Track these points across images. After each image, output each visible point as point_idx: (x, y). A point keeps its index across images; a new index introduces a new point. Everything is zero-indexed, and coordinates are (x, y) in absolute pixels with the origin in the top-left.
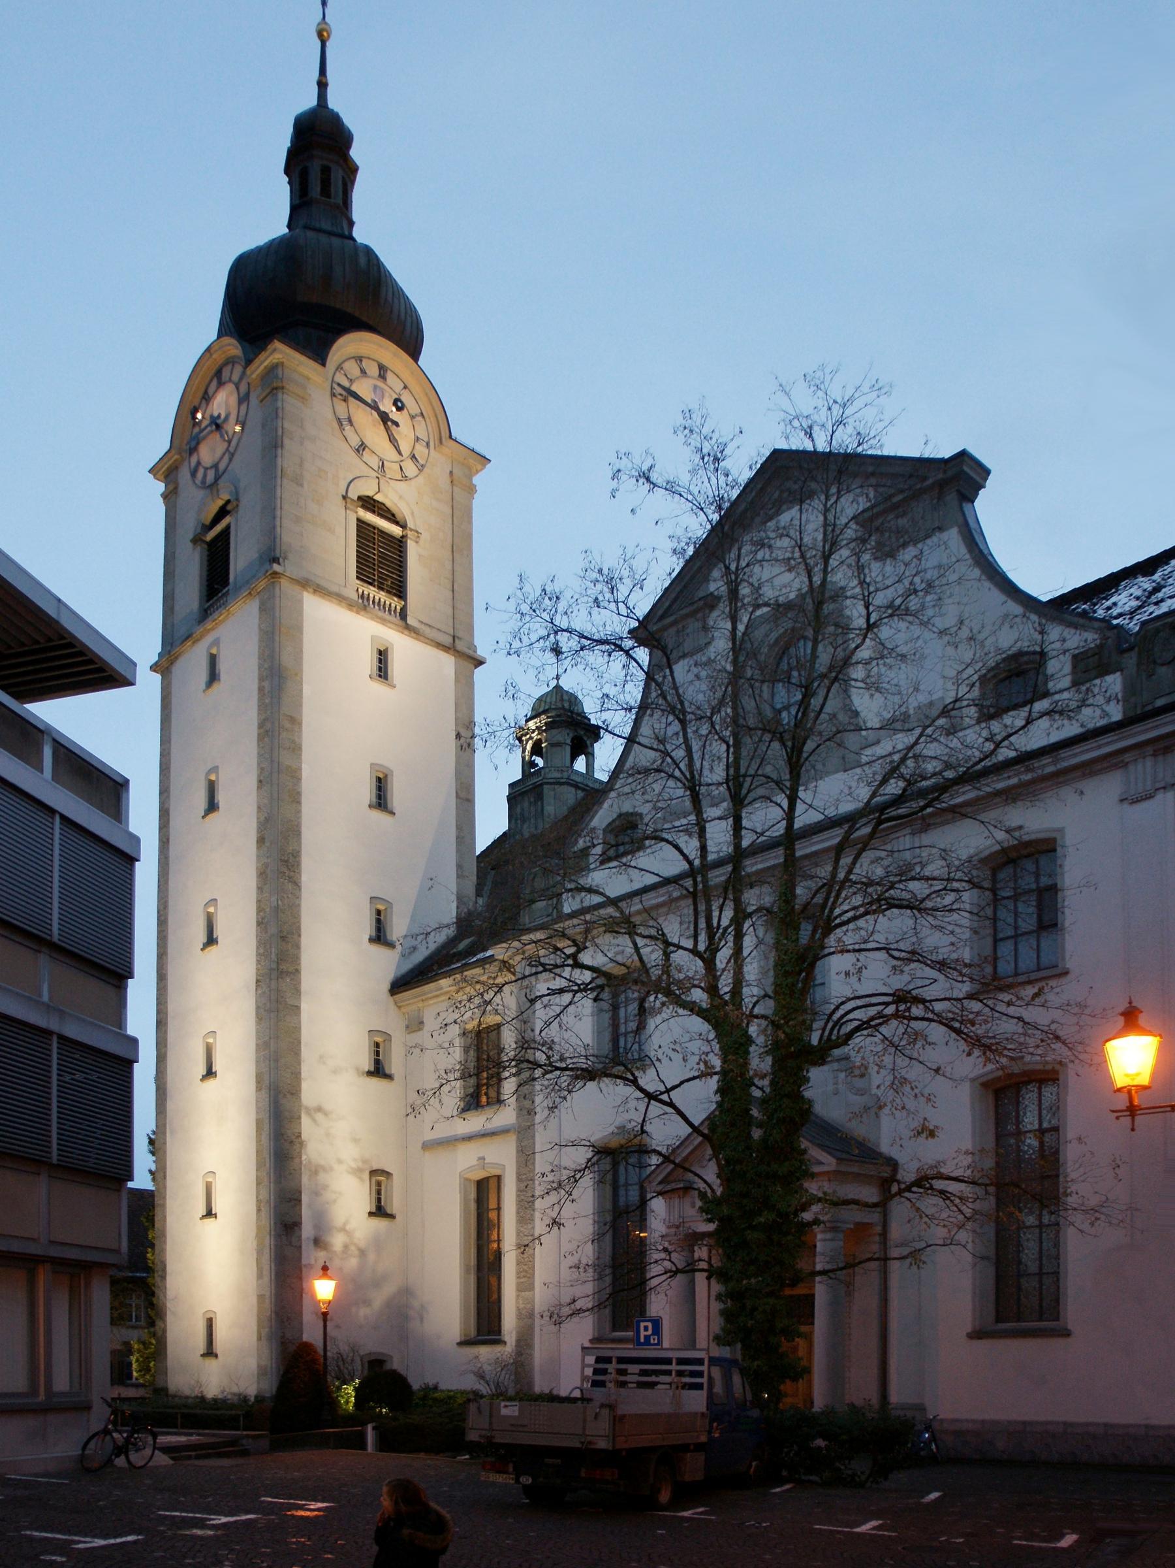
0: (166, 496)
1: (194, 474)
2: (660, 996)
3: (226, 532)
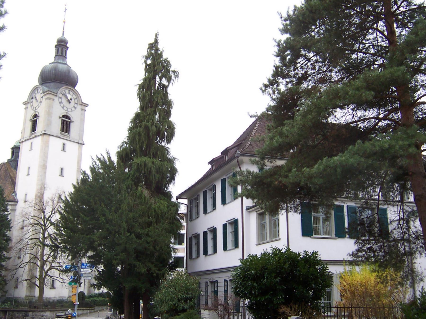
3: (37, 120)
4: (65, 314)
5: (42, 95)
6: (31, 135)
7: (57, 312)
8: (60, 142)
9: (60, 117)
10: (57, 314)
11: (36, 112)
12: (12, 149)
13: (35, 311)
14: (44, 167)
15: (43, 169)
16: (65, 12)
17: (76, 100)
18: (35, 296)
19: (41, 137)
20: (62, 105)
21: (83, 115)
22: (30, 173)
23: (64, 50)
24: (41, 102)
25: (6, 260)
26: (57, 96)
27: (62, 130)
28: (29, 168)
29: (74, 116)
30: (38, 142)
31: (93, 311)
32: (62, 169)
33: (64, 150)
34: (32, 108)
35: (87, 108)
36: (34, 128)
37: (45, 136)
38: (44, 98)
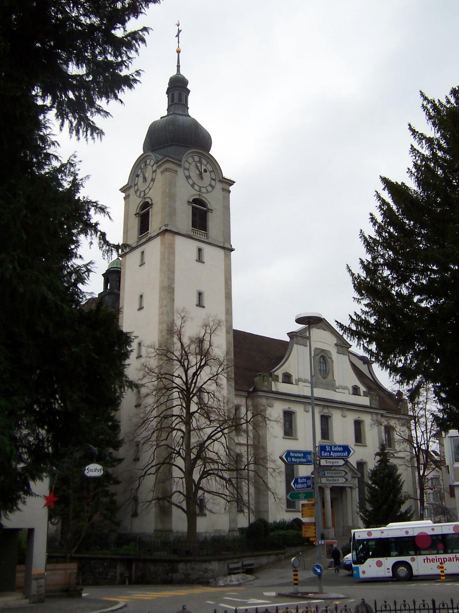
0: (125, 198)
1: (136, 192)
2: (437, 398)
3: (148, 212)
4: (243, 566)
5: (155, 166)
6: (140, 239)
7: (229, 561)
8: (193, 245)
9: (189, 202)
10: (232, 566)
11: (145, 198)
12: (104, 275)
13: (190, 561)
14: (169, 290)
15: (168, 293)
16: (178, 36)
17: (213, 174)
18: (172, 531)
19: (158, 239)
20: (191, 182)
21: (226, 200)
22: (144, 305)
23: (184, 94)
24: (153, 180)
25: (115, 464)
26: (180, 166)
27: (194, 225)
28: (141, 296)
29: (212, 199)
30: (154, 249)
31: (283, 556)
32: (200, 294)
33: (200, 259)
34: (138, 194)
35: (231, 188)
36: (144, 226)
37: (168, 236)
38: (159, 171)
